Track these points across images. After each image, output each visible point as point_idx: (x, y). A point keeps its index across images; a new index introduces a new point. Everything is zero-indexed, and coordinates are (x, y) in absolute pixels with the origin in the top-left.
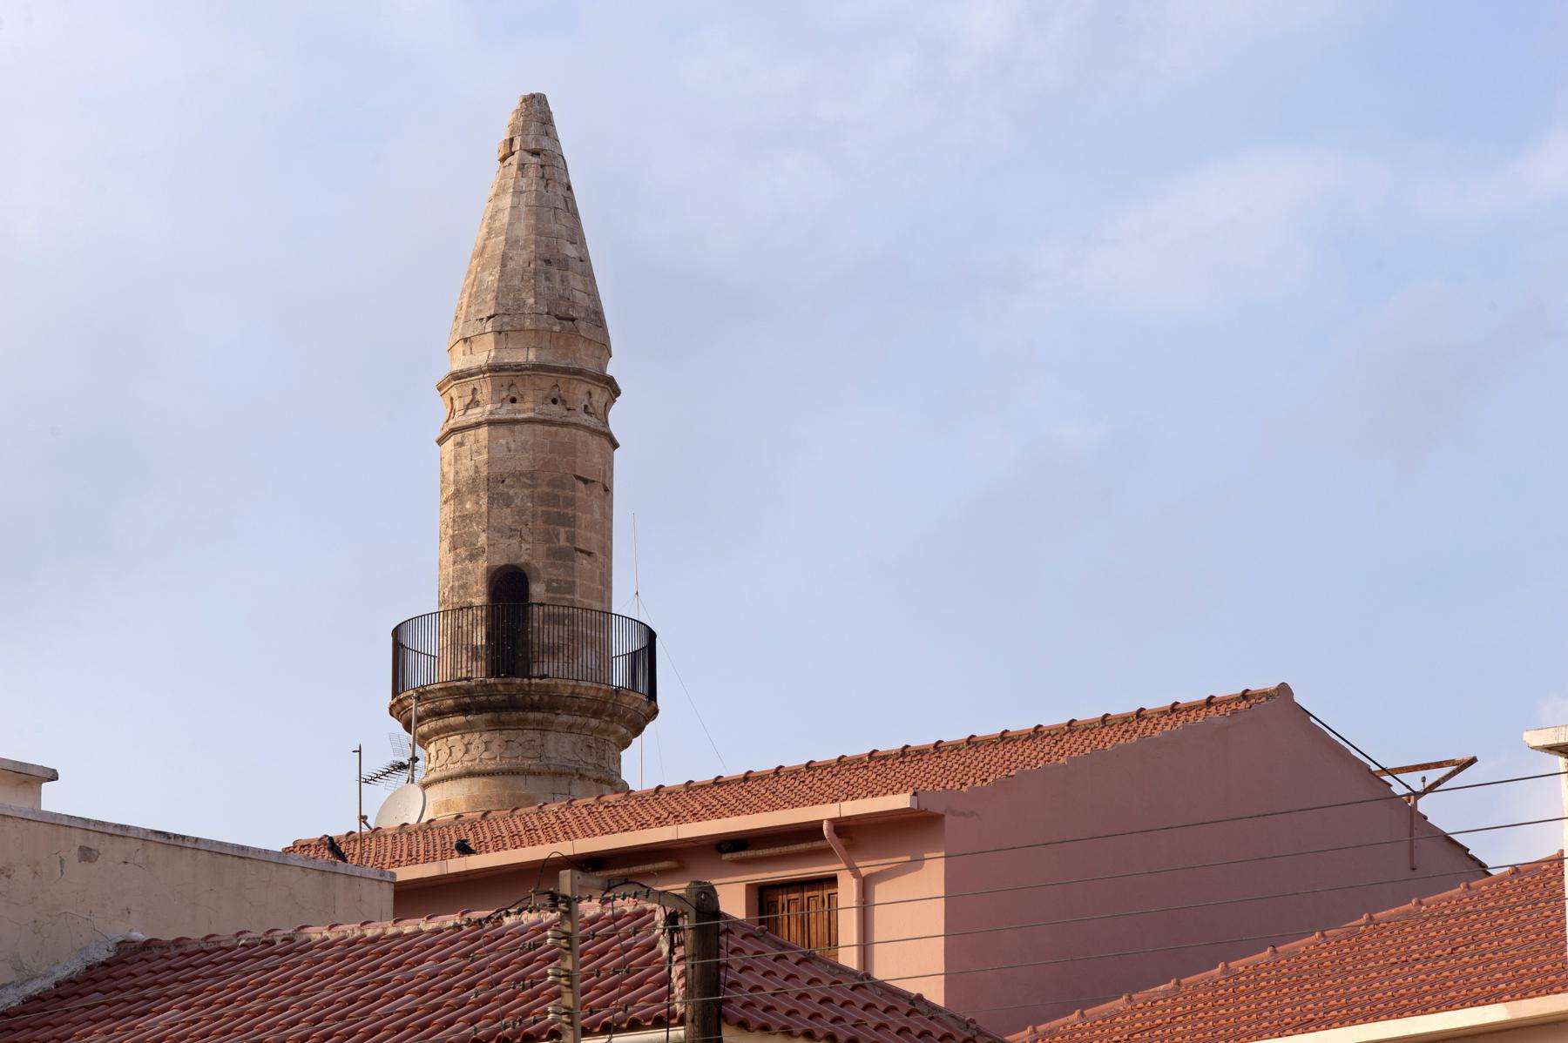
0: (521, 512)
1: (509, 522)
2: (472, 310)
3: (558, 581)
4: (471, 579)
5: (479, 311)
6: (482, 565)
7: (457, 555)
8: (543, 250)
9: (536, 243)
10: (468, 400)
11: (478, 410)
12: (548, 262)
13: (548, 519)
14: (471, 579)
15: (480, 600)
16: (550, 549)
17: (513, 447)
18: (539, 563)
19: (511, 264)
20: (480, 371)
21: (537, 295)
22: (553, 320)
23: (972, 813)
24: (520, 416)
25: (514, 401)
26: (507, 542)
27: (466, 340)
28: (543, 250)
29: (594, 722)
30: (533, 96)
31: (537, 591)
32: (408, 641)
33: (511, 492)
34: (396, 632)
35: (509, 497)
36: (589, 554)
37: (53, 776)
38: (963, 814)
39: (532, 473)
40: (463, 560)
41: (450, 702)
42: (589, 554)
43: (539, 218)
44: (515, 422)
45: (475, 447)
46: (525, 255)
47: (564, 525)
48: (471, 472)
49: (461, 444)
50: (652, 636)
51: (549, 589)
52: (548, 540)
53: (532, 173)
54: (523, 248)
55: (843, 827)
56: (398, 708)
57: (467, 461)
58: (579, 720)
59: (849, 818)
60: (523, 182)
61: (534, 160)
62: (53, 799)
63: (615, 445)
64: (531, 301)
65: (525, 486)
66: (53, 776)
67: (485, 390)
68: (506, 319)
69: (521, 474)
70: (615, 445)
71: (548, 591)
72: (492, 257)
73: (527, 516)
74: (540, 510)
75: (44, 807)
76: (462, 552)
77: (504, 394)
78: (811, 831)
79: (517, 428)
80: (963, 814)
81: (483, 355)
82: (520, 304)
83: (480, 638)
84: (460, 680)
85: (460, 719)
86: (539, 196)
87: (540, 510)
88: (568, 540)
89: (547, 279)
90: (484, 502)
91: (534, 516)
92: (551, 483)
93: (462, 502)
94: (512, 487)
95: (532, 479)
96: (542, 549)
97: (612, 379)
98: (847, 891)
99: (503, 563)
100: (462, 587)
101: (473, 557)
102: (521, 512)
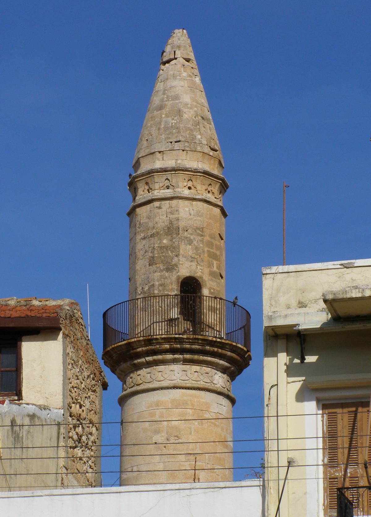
1: (190, 253)
3: (214, 289)
4: (168, 281)
17: (192, 212)
24: (197, 197)
26: (190, 264)
30: (247, 365)
32: (113, 324)
33: (192, 237)
34: (105, 315)
35: (190, 240)
39: (202, 228)
40: (162, 271)
41: (167, 346)
45: (169, 210)
47: (216, 260)
54: (191, 108)
68: (187, 144)
69: (197, 228)
70: (227, 188)
74: (206, 249)
77: (185, 184)
79: (194, 203)
87: (206, 249)
88: (217, 268)
94: (191, 234)
95: (202, 231)
96: (206, 270)
99: (188, 274)
102: (197, 248)
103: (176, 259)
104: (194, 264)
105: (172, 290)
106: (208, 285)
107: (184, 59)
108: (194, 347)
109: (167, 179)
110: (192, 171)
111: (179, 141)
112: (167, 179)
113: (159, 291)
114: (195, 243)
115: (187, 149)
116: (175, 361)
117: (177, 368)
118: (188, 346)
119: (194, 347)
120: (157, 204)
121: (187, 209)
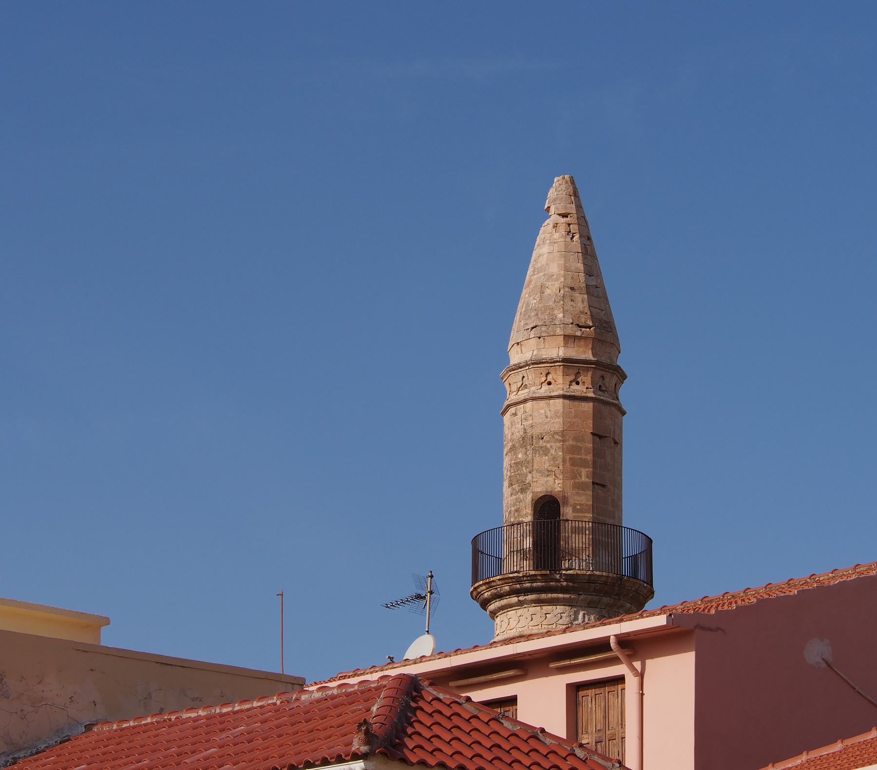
0: (554, 459)
2: (522, 323)
5: (527, 324)
6: (528, 498)
7: (513, 489)
8: (569, 281)
9: (565, 276)
10: (519, 384)
11: (526, 391)
12: (572, 289)
13: (573, 462)
14: (522, 505)
15: (529, 518)
16: (575, 483)
17: (549, 414)
18: (569, 493)
19: (547, 292)
20: (527, 364)
21: (564, 312)
22: (575, 328)
23: (718, 629)
24: (553, 394)
25: (549, 383)
27: (518, 344)
28: (569, 281)
29: (606, 600)
31: (567, 512)
33: (548, 446)
34: (475, 541)
35: (546, 448)
36: (603, 486)
37: (107, 621)
38: (710, 630)
40: (517, 493)
41: (507, 588)
42: (603, 486)
43: (567, 260)
44: (551, 397)
46: (557, 285)
48: (522, 433)
49: (515, 414)
50: (650, 541)
51: (575, 510)
52: (574, 477)
53: (562, 229)
54: (557, 280)
55: (625, 641)
56: (475, 593)
57: (519, 426)
58: (595, 598)
59: (628, 634)
60: (556, 235)
61: (563, 220)
62: (109, 638)
63: (623, 413)
64: (561, 315)
65: (558, 441)
66: (107, 621)
67: (586, 378)
68: (544, 329)
70: (623, 413)
71: (574, 511)
72: (535, 287)
73: (560, 461)
75: (103, 644)
76: (516, 487)
78: (602, 645)
79: (552, 401)
80: (710, 630)
81: (556, 350)
82: (553, 318)
83: (528, 543)
84: (512, 573)
85: (514, 599)
86: (566, 246)
89: (572, 300)
90: (530, 452)
91: (564, 461)
92: (575, 439)
93: (516, 454)
94: (548, 442)
97: (619, 367)
98: (631, 682)
100: (516, 511)
101: (523, 491)
102: (554, 459)
103: (529, 476)
104: (551, 479)
105: (526, 515)
106: (571, 501)
107: (559, 215)
108: (534, 585)
109: (603, 377)
110: (547, 362)
111: (535, 327)
112: (603, 377)
113: (515, 518)
114: (553, 452)
115: (543, 335)
116: (520, 604)
117: (526, 612)
118: (528, 585)
119: (534, 585)
120: (512, 410)
121: (543, 411)
